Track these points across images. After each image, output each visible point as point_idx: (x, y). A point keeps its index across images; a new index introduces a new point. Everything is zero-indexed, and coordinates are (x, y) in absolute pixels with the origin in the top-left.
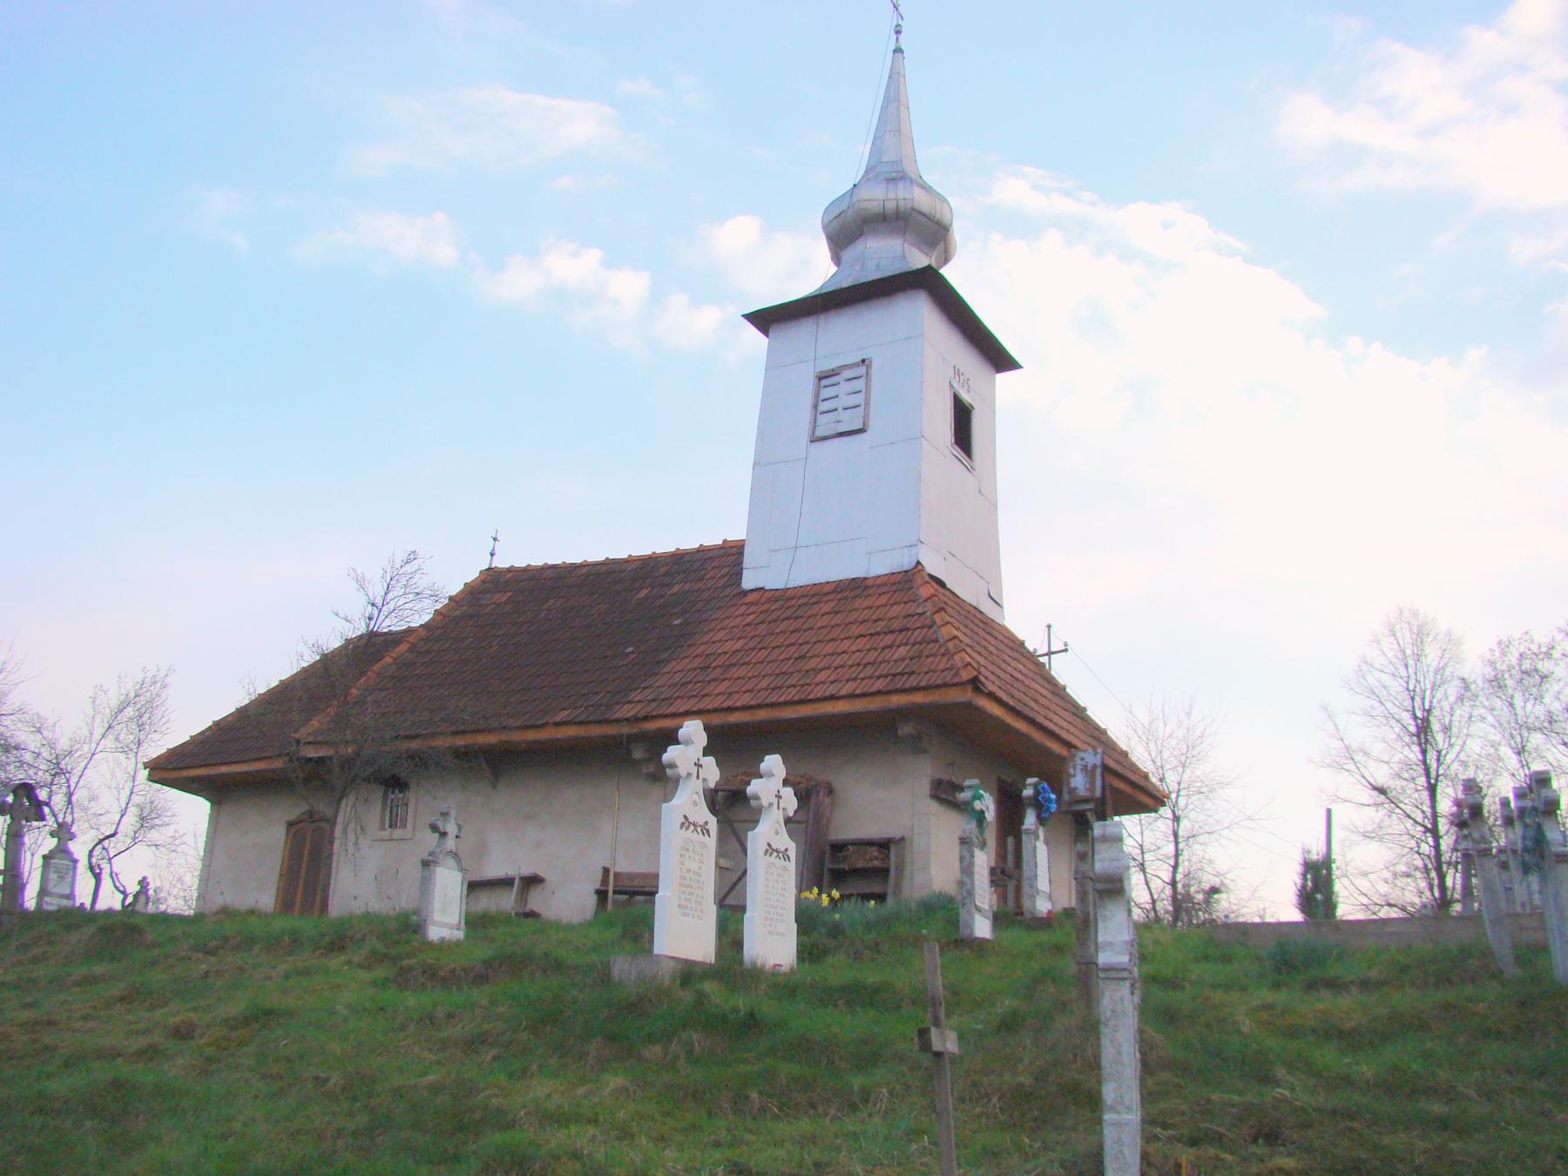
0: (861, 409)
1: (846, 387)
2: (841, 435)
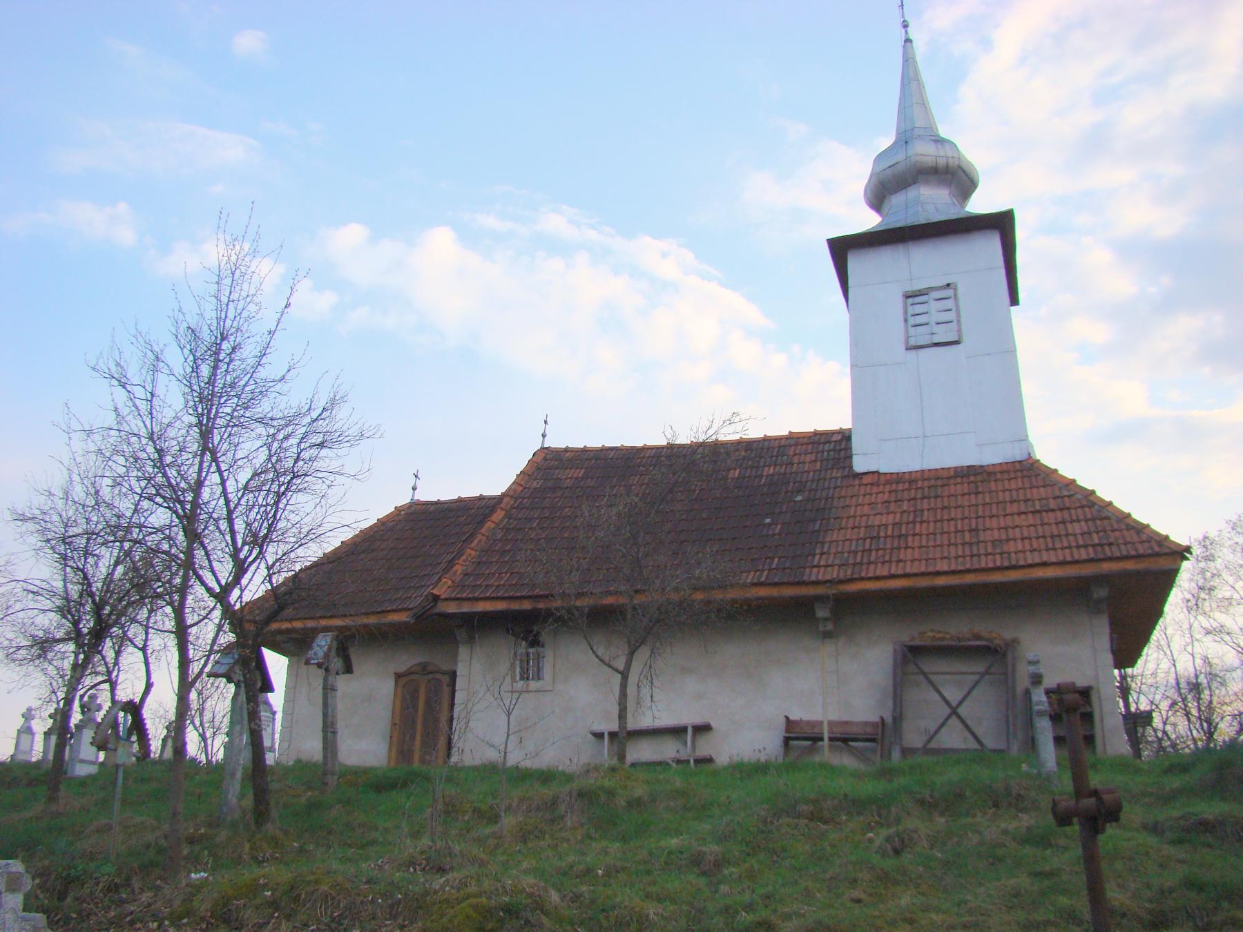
0: (954, 325)
1: (934, 306)
2: (936, 345)
